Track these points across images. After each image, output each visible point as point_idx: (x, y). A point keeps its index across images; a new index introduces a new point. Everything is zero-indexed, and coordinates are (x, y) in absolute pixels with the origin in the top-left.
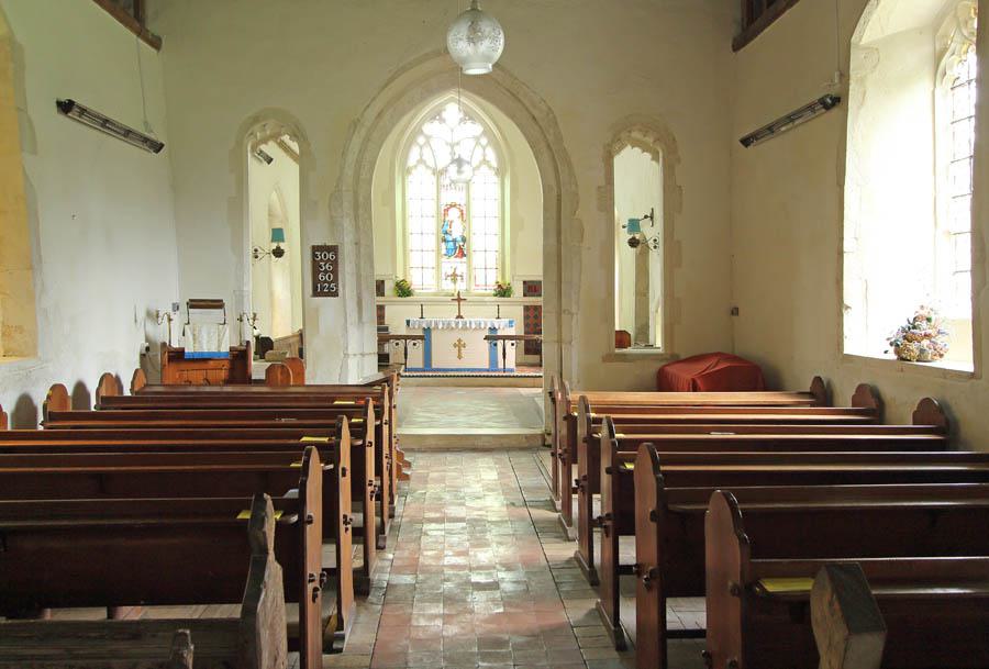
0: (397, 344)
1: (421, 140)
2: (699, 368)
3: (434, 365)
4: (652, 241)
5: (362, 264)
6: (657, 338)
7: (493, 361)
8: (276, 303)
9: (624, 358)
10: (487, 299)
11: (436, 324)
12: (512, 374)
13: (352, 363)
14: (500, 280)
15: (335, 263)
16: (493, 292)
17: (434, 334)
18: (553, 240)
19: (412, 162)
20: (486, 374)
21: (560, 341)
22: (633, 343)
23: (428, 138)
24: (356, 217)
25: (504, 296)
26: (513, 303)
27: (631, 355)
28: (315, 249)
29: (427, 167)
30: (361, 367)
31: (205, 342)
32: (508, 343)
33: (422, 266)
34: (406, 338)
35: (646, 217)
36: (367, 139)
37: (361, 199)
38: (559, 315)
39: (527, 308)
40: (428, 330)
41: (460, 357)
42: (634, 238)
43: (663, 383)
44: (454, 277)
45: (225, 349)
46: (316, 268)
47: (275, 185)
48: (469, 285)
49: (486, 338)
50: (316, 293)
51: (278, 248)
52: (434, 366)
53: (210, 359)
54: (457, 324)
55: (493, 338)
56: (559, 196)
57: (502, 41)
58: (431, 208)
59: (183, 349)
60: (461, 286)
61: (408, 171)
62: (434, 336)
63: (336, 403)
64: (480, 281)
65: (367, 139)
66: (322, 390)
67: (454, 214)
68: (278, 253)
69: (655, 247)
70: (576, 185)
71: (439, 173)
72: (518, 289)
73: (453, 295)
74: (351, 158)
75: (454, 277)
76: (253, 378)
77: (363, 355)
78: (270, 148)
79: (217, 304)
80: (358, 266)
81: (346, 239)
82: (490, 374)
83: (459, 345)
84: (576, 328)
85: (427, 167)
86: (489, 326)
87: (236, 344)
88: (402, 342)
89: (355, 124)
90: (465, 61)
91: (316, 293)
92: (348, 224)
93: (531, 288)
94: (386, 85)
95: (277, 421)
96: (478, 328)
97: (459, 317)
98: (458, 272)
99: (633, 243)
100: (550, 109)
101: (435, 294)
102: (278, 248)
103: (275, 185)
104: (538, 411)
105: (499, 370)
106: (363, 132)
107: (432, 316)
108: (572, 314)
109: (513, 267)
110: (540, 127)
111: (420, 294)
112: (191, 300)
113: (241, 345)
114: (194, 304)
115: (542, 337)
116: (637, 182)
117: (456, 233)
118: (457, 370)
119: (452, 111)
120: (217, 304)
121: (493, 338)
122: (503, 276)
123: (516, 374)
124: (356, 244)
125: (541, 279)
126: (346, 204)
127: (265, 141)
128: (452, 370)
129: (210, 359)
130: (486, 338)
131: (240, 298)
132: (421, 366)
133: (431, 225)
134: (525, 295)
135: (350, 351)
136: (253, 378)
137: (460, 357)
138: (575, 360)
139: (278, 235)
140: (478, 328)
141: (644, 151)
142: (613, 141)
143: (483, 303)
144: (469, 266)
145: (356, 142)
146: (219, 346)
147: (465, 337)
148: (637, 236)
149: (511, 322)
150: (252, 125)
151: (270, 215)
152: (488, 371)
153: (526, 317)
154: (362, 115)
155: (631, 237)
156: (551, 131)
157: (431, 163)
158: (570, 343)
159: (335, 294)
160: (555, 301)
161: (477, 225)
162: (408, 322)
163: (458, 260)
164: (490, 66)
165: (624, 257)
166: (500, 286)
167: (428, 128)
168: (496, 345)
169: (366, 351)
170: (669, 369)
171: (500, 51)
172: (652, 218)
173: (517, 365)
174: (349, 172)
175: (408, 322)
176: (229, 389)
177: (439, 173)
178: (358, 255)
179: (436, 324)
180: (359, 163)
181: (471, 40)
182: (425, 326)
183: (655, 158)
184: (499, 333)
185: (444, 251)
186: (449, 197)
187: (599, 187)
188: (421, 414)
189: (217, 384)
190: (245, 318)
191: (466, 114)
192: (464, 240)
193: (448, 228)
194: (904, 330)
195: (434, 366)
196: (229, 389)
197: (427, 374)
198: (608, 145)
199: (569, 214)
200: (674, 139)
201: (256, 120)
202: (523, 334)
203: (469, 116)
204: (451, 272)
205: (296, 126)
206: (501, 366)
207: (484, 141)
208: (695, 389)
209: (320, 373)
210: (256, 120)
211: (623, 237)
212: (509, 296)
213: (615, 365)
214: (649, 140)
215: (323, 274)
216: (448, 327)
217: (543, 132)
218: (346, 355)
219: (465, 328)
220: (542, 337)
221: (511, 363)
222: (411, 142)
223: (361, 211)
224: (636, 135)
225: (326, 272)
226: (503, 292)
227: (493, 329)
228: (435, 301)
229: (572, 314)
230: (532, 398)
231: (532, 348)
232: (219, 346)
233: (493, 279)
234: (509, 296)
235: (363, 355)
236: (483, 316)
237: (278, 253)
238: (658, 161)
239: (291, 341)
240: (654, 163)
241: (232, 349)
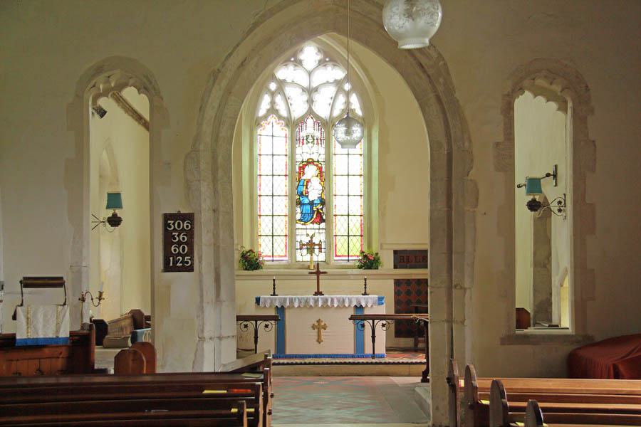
0: (246, 326)
1: (273, 86)
2: (622, 351)
3: (289, 350)
4: (555, 203)
5: (221, 232)
6: (565, 318)
7: (359, 344)
8: (115, 277)
9: (527, 339)
10: (349, 271)
11: (292, 301)
12: (383, 361)
13: (208, 347)
14: (365, 249)
15: (190, 234)
16: (358, 264)
17: (288, 314)
18: (442, 206)
19: (262, 111)
20: (351, 360)
21: (450, 321)
22: (532, 325)
23: (282, 84)
24: (215, 180)
25: (370, 268)
26: (384, 276)
27: (535, 336)
28: (167, 217)
29: (280, 117)
30: (217, 353)
31: (40, 326)
32: (379, 324)
33: (272, 232)
34: (256, 318)
35: (548, 175)
36: (228, 92)
37: (220, 160)
38: (450, 288)
39: (398, 283)
40: (281, 310)
41: (319, 341)
42: (534, 200)
43: (575, 367)
44: (310, 247)
45: (64, 333)
46: (168, 239)
47: (117, 145)
48: (328, 255)
49: (352, 318)
50: (167, 268)
51: (115, 215)
52: (288, 352)
53: (44, 346)
54: (316, 301)
55: (359, 317)
56: (450, 155)
57: (440, 14)
58: (281, 165)
59: (14, 336)
60: (320, 257)
61: (257, 123)
62: (289, 317)
63: (206, 392)
64: (342, 250)
65: (228, 92)
66: (174, 379)
67: (311, 171)
68: (115, 221)
69: (560, 210)
70: (470, 141)
71: (293, 124)
72: (387, 260)
73: (309, 268)
74: (210, 113)
75: (310, 247)
76: (96, 367)
77: (220, 338)
78: (104, 102)
79: (57, 282)
80: (216, 236)
81: (203, 205)
82: (356, 360)
83: (319, 327)
84: (471, 305)
85: (280, 117)
86: (354, 303)
87: (77, 328)
88: (251, 324)
89: (215, 75)
90: (401, 36)
91: (167, 268)
92: (205, 188)
93: (404, 258)
94: (251, 31)
95: (146, 413)
96: (342, 306)
97: (318, 293)
98: (316, 241)
99: (533, 206)
100: (440, 55)
101: (287, 267)
102: (115, 215)
103: (117, 145)
104: (422, 404)
105: (367, 356)
106: (224, 83)
107: (284, 296)
108: (465, 290)
109: (382, 233)
110: (429, 76)
111: (269, 267)
112: (25, 278)
113: (82, 328)
114: (28, 283)
115: (427, 317)
116: (541, 134)
117: (314, 195)
118: (316, 356)
119: (310, 53)
120: (57, 282)
121: (359, 317)
122: (369, 245)
123: (387, 360)
124: (214, 211)
125: (427, 247)
126: (203, 166)
127: (105, 94)
128: (310, 356)
129: (44, 346)
130: (352, 318)
131: (79, 274)
132: (351, 352)
133: (282, 186)
134: (395, 267)
135: (206, 335)
136: (96, 367)
137: (319, 341)
138: (470, 342)
139: (114, 200)
140: (342, 306)
141: (535, 96)
142: (513, 91)
143: (345, 276)
144: (328, 231)
145: (216, 94)
146: (57, 331)
147: (326, 317)
148: (537, 198)
149: (380, 299)
150: (94, 76)
151: (100, 176)
152: (353, 356)
153: (397, 293)
154: (223, 65)
155: (530, 198)
156: (441, 80)
157: (284, 113)
158: (463, 323)
159: (191, 269)
160: (445, 275)
161: (339, 185)
162: (258, 300)
163: (316, 226)
164: (427, 41)
165: (524, 220)
166: (365, 256)
167: (283, 73)
168: (363, 326)
169: (225, 333)
170: (581, 353)
171: (437, 25)
172: (555, 176)
173: (388, 350)
174: (207, 129)
175: (258, 300)
176: (65, 380)
177: (293, 124)
178: (216, 224)
179: (292, 301)
180: (218, 121)
181: (410, 15)
182: (277, 304)
183: (563, 108)
184: (367, 312)
185: (298, 216)
186: (304, 152)
187: (497, 144)
188: (282, 408)
189: (51, 375)
190: (88, 299)
191: (326, 54)
192: (323, 202)
193: (303, 189)
194: (160, 92)
195: (288, 352)
196: (65, 380)
197: (281, 361)
198: (508, 95)
199: (459, 167)
200: (587, 87)
201: (99, 70)
202: (392, 312)
203: (329, 58)
204: (306, 240)
205: (146, 77)
206: (368, 350)
207: (347, 87)
208: (617, 376)
209: (173, 359)
210: (99, 70)
211: (522, 198)
212: (377, 268)
213: (516, 348)
214: (557, 88)
215: (177, 243)
216: (305, 305)
217: (431, 82)
218: (202, 339)
219: (325, 307)
220: (427, 317)
221: (381, 348)
222: (263, 88)
223: (220, 173)
224: (540, 82)
225: (179, 243)
226: (369, 262)
227: (359, 308)
228: (292, 272)
229: (465, 290)
230: (411, 389)
231: (409, 330)
232: (57, 331)
233: (356, 247)
234: (377, 268)
235: (220, 338)
236: (347, 293)
237: (115, 221)
238: (565, 110)
239: (123, 323)
240: (560, 113)
241: (72, 333)
